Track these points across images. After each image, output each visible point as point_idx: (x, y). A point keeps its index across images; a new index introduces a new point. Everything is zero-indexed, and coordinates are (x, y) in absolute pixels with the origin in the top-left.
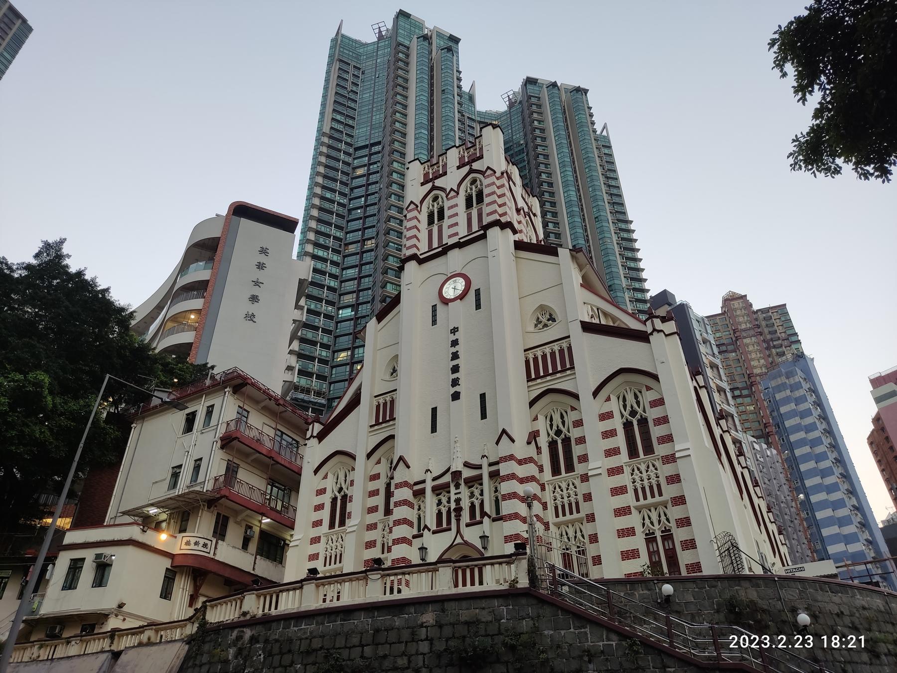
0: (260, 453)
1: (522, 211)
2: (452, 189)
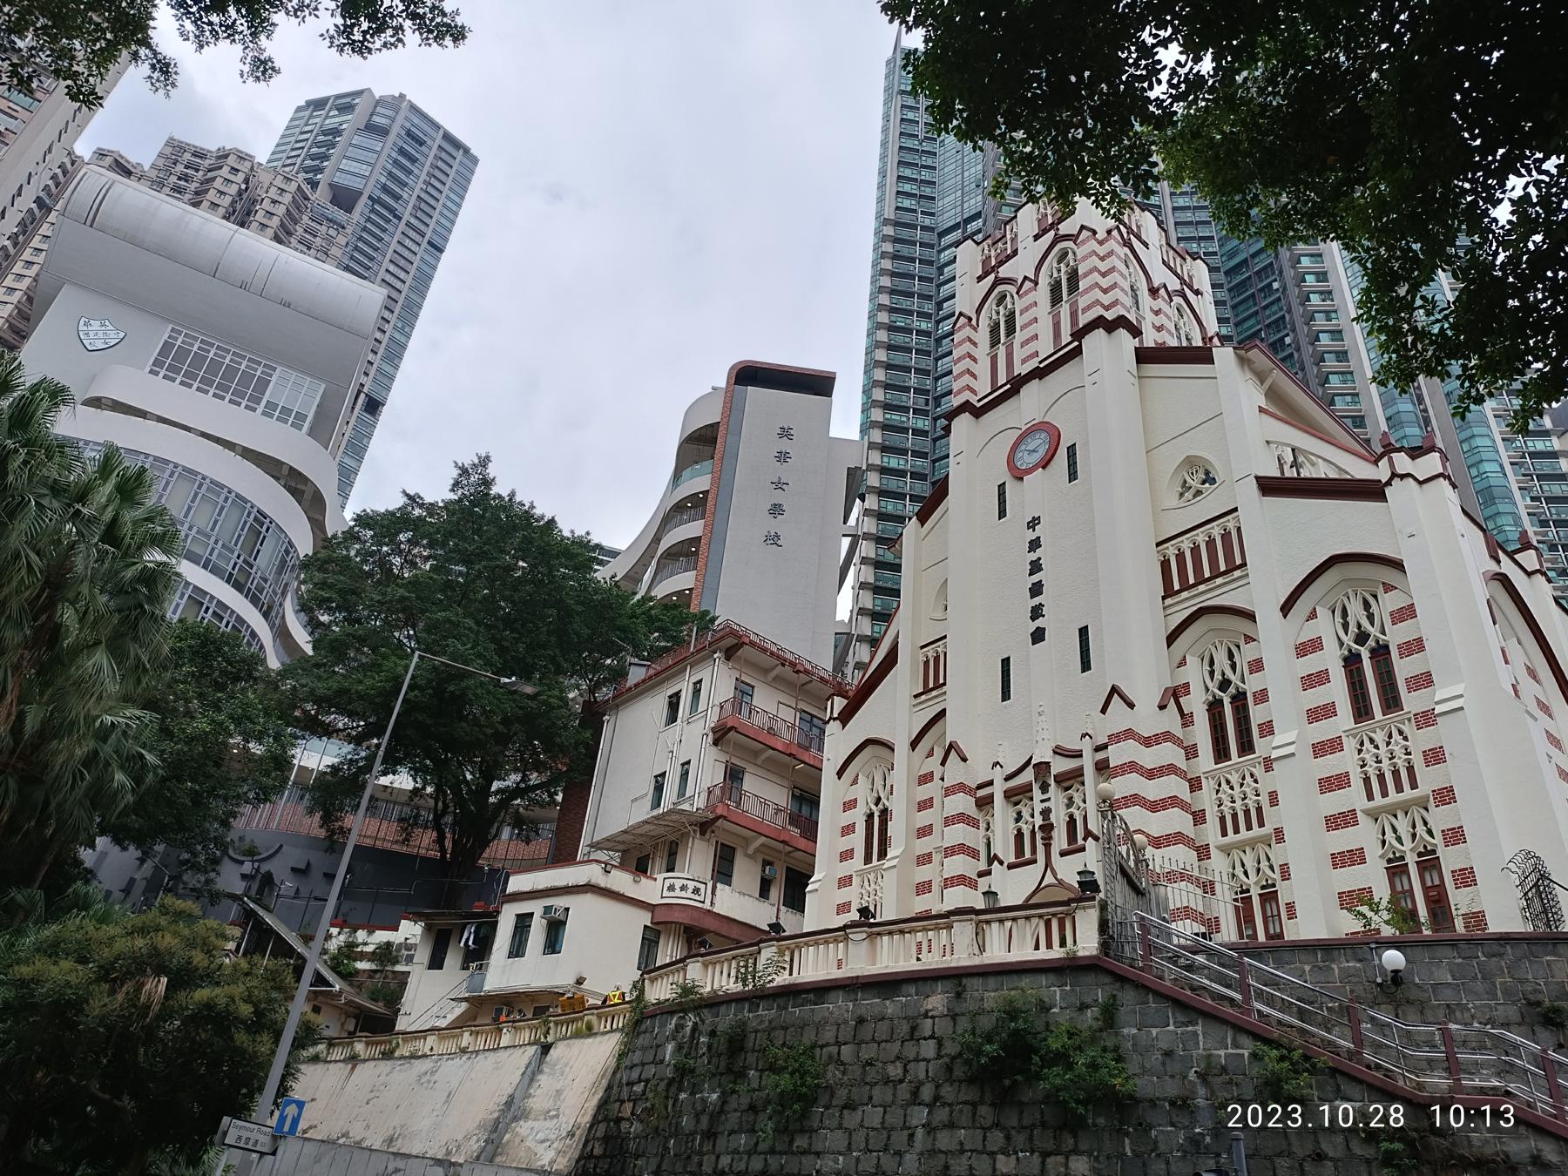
0: (774, 749)
1: (1162, 292)
2: (1026, 278)
